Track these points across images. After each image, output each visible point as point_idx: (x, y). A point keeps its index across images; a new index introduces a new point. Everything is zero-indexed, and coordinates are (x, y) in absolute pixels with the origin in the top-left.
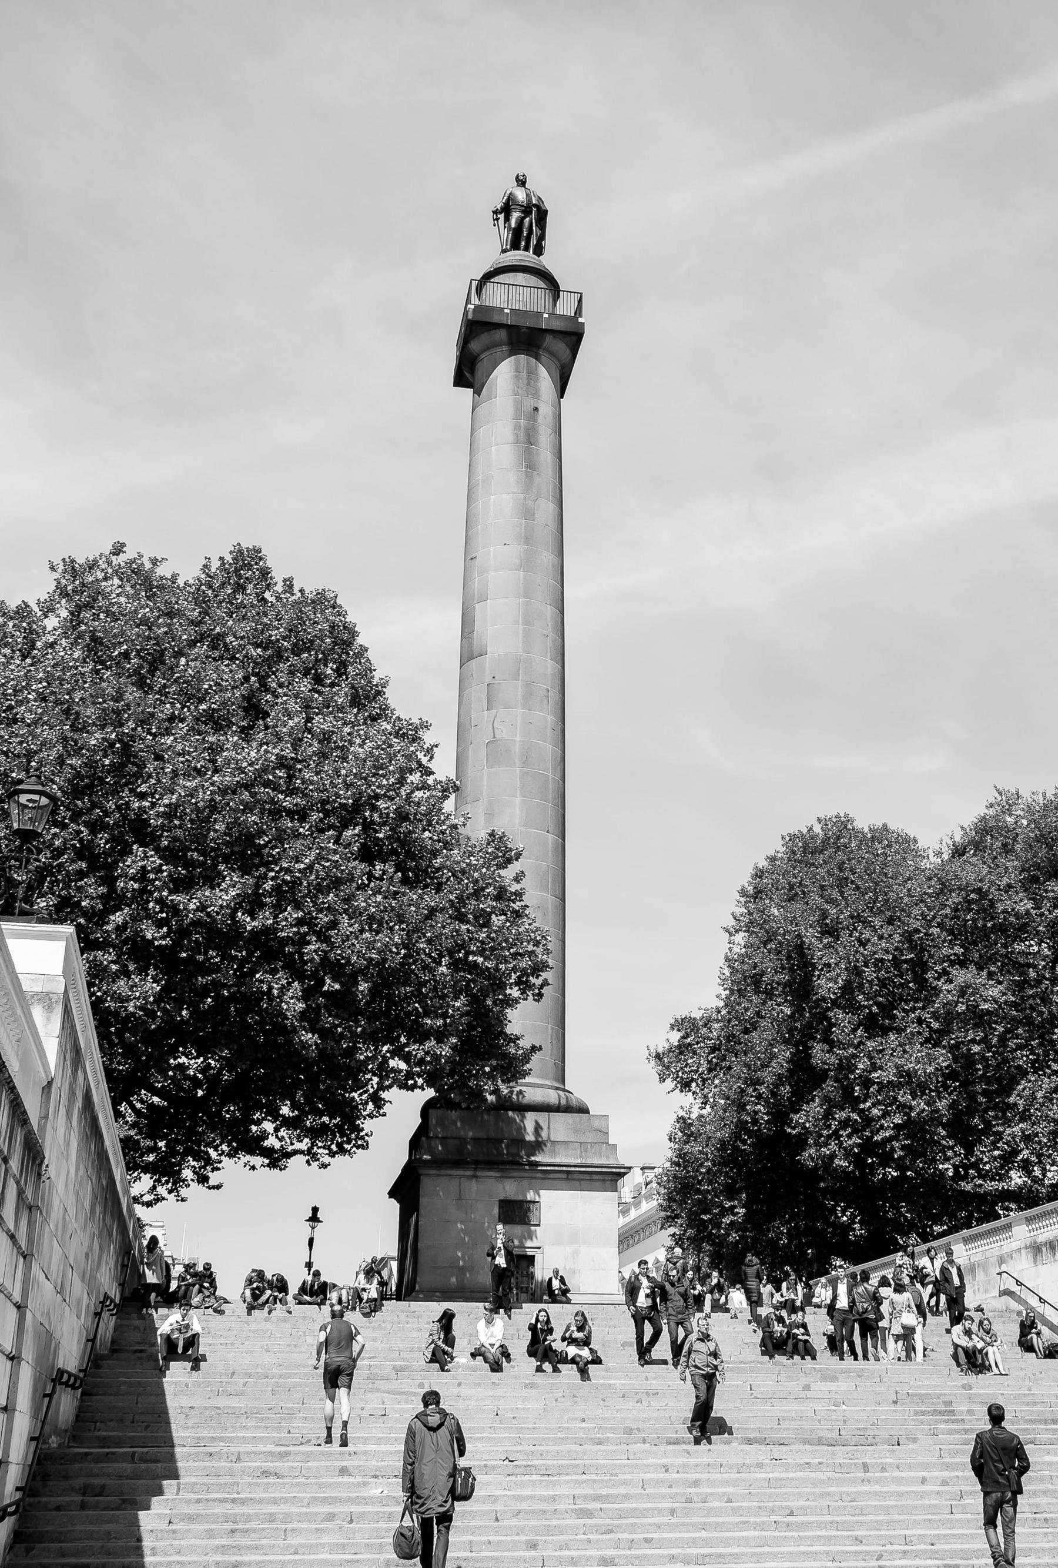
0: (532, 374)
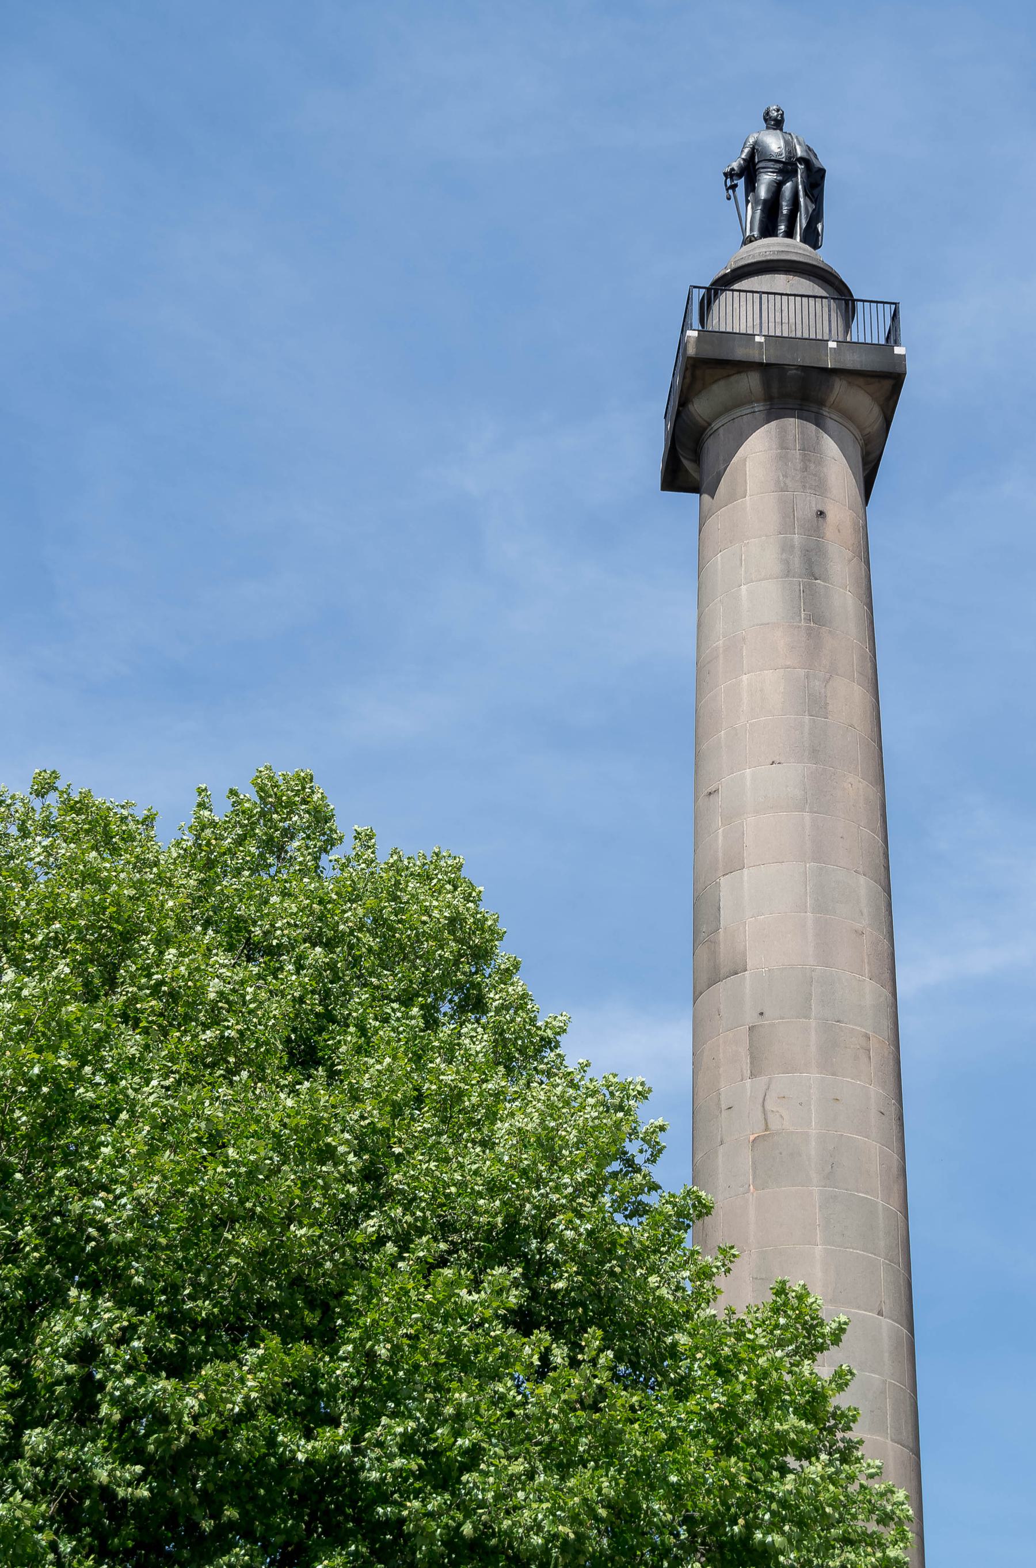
0: (810, 452)
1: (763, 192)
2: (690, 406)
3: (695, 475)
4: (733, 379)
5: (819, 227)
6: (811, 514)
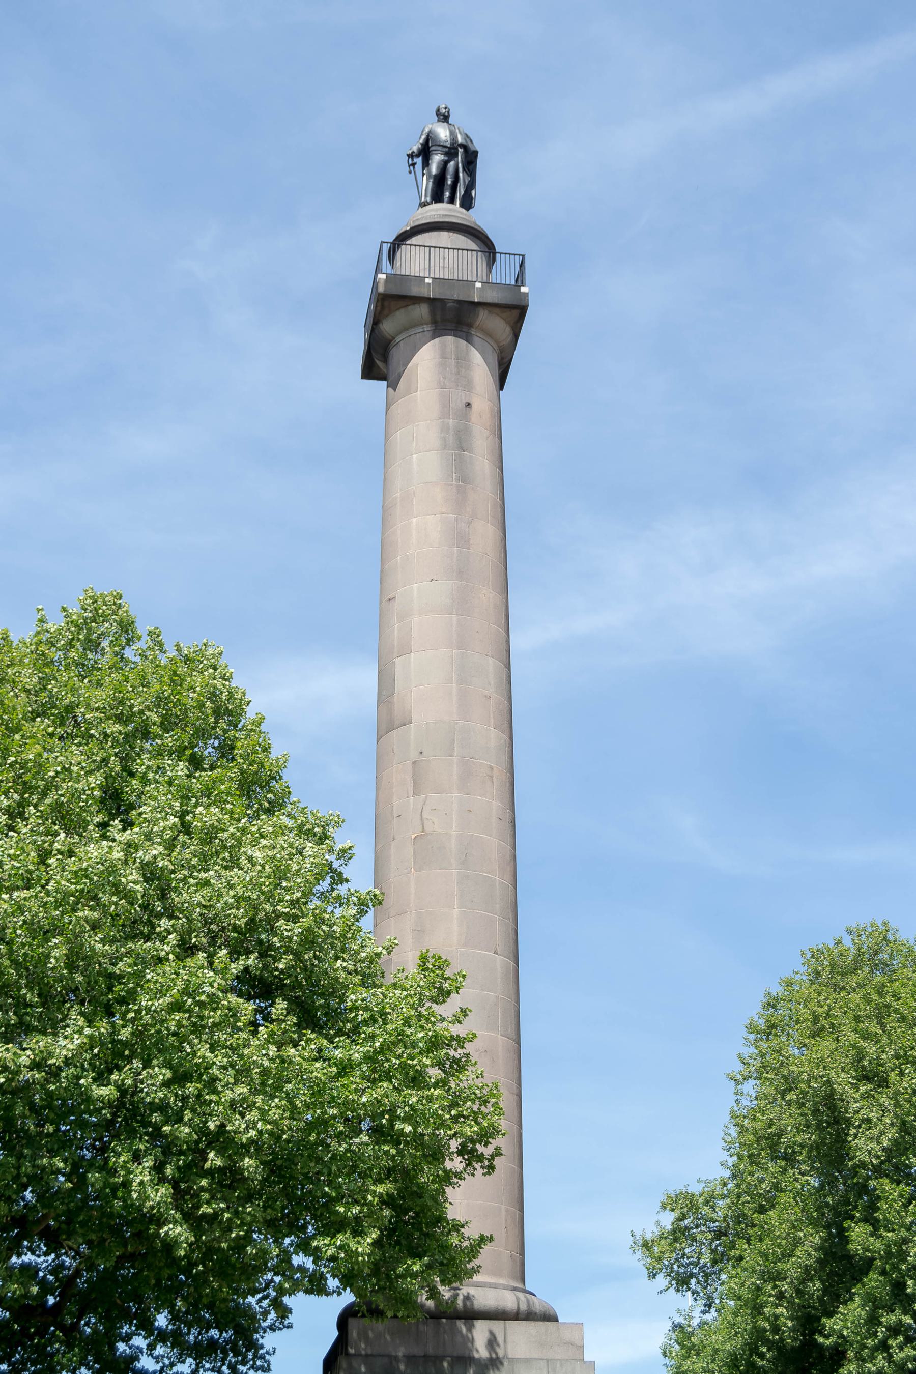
0: (462, 361)
1: (434, 169)
2: (381, 325)
3: (385, 371)
4: (410, 308)
5: (473, 193)
6: (461, 405)
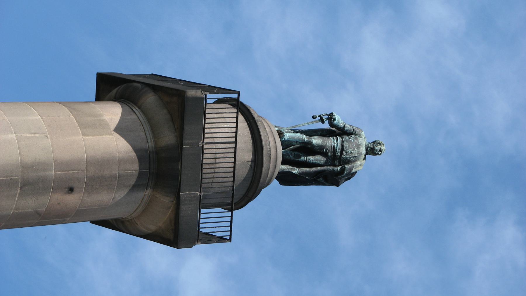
1: (316, 141)
